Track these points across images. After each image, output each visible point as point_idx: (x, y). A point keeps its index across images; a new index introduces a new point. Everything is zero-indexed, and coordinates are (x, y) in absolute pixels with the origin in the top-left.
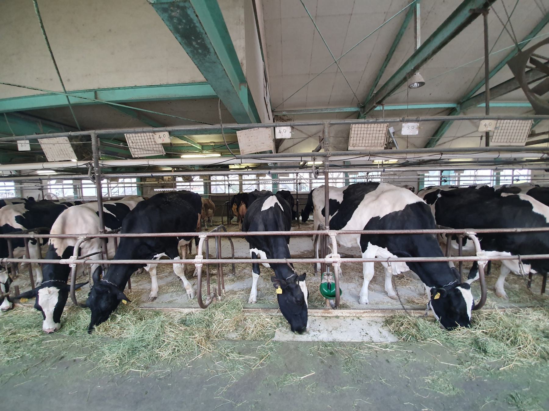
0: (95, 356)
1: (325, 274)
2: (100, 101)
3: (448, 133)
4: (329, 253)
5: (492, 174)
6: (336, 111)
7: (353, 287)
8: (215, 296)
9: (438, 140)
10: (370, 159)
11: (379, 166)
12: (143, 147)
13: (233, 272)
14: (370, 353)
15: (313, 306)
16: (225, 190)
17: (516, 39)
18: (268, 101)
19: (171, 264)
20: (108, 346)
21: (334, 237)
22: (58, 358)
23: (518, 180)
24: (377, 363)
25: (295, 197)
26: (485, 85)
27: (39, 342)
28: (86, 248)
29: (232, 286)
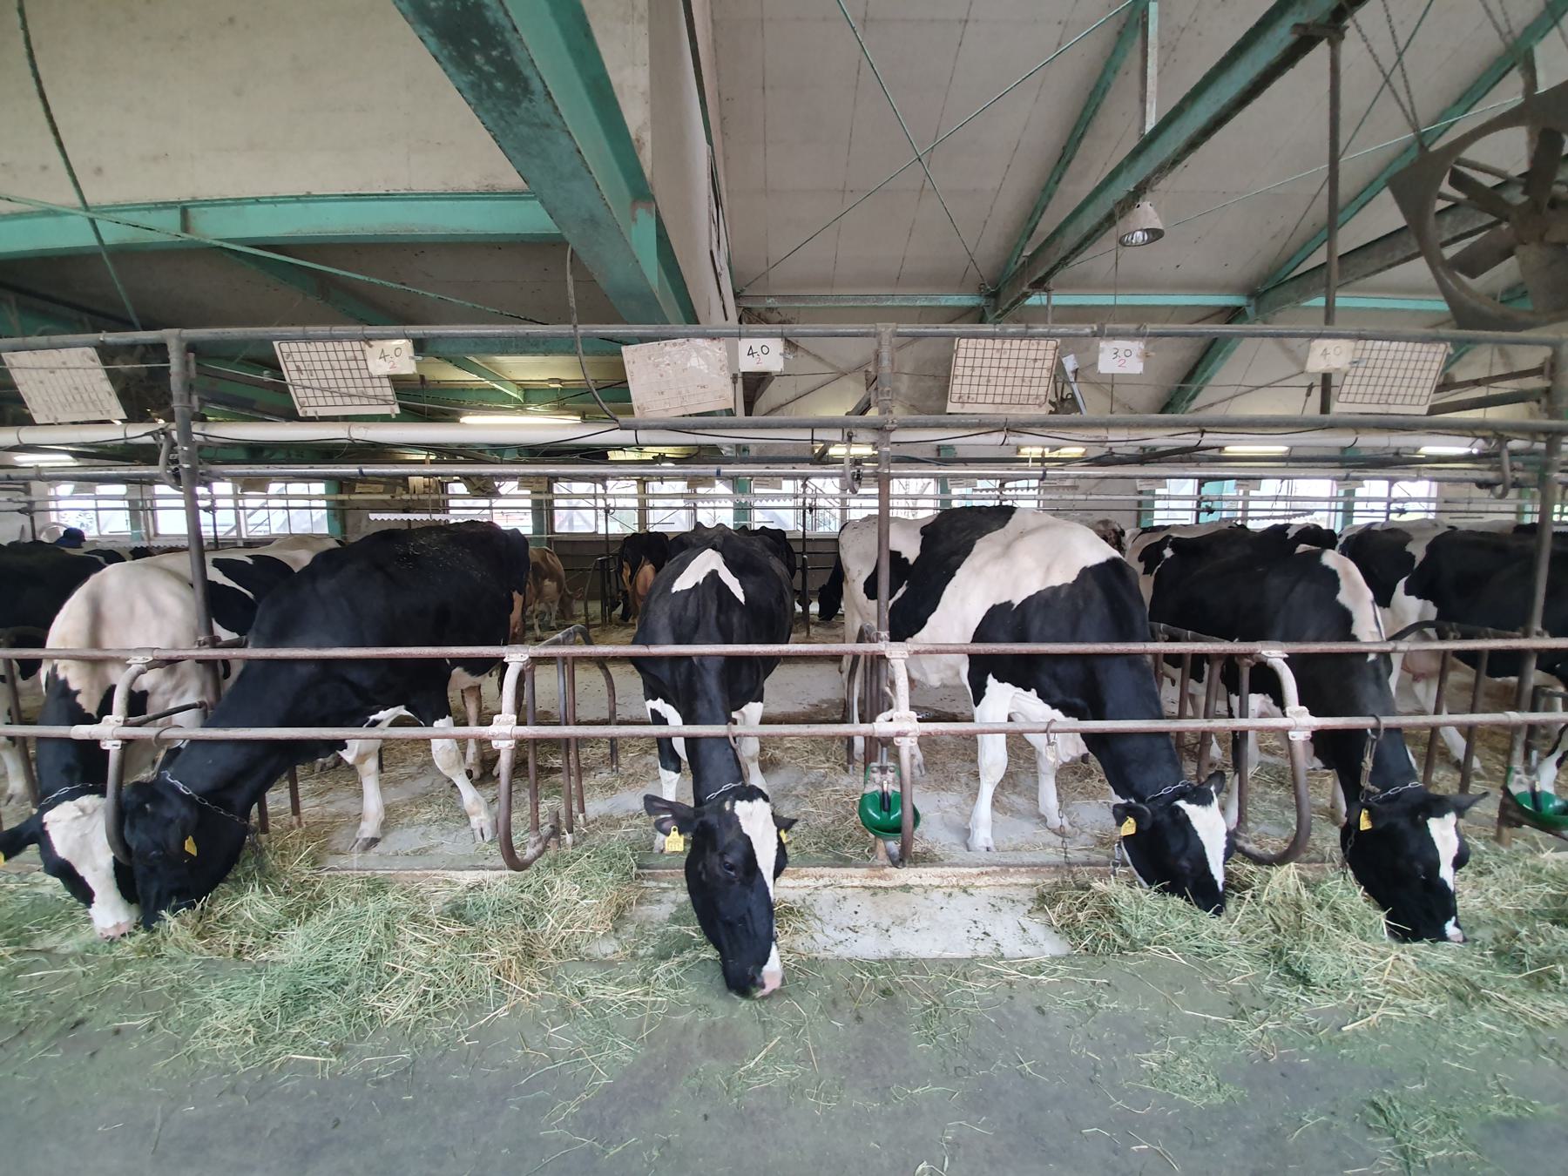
0: (182, 1015)
1: (875, 769)
2: (196, 239)
3: (1225, 375)
4: (886, 705)
5: (1335, 495)
6: (918, 303)
7: (951, 802)
8: (556, 832)
9: (1194, 397)
10: (1006, 442)
11: (1030, 464)
12: (333, 384)
13: (612, 763)
14: (993, 990)
15: (839, 858)
16: (596, 525)
17: (1414, 114)
18: (722, 262)
19: (427, 741)
20: (223, 986)
21: (902, 662)
22: (66, 1023)
23: (1402, 512)
24: (1010, 1017)
25: (797, 548)
26: (1326, 244)
27: (9, 974)
28: (164, 693)
29: (609, 802)
